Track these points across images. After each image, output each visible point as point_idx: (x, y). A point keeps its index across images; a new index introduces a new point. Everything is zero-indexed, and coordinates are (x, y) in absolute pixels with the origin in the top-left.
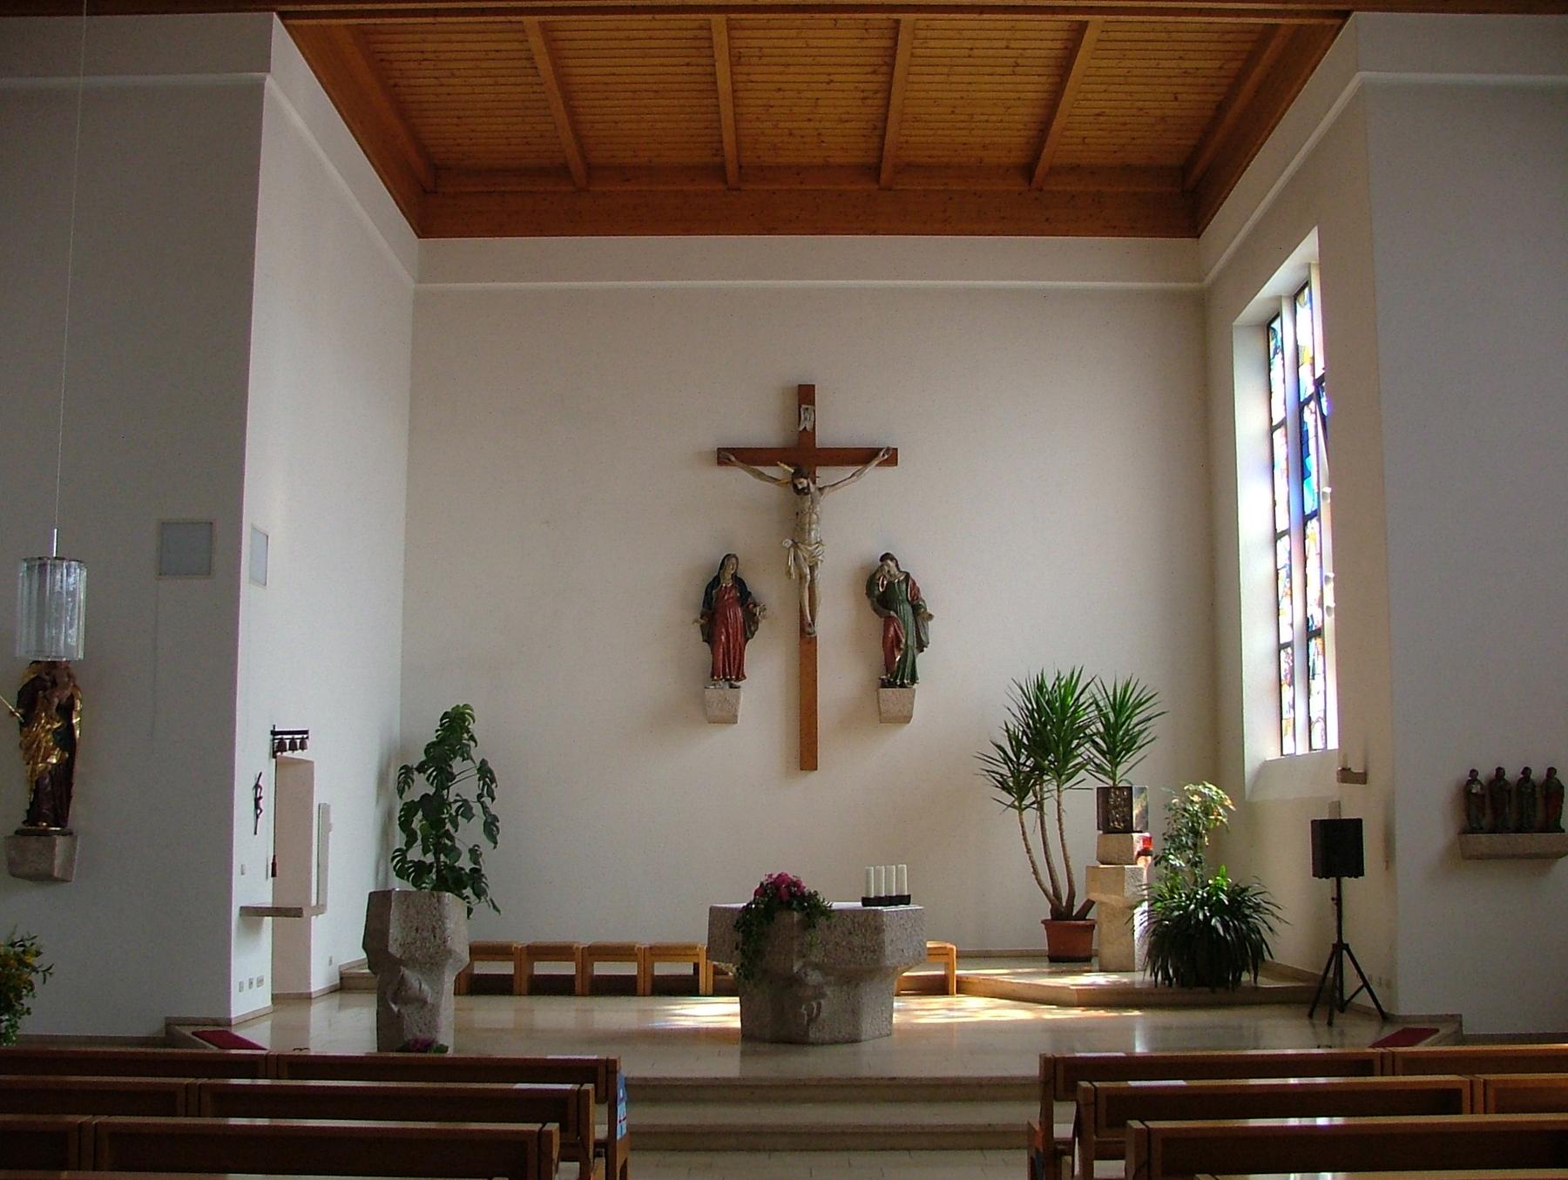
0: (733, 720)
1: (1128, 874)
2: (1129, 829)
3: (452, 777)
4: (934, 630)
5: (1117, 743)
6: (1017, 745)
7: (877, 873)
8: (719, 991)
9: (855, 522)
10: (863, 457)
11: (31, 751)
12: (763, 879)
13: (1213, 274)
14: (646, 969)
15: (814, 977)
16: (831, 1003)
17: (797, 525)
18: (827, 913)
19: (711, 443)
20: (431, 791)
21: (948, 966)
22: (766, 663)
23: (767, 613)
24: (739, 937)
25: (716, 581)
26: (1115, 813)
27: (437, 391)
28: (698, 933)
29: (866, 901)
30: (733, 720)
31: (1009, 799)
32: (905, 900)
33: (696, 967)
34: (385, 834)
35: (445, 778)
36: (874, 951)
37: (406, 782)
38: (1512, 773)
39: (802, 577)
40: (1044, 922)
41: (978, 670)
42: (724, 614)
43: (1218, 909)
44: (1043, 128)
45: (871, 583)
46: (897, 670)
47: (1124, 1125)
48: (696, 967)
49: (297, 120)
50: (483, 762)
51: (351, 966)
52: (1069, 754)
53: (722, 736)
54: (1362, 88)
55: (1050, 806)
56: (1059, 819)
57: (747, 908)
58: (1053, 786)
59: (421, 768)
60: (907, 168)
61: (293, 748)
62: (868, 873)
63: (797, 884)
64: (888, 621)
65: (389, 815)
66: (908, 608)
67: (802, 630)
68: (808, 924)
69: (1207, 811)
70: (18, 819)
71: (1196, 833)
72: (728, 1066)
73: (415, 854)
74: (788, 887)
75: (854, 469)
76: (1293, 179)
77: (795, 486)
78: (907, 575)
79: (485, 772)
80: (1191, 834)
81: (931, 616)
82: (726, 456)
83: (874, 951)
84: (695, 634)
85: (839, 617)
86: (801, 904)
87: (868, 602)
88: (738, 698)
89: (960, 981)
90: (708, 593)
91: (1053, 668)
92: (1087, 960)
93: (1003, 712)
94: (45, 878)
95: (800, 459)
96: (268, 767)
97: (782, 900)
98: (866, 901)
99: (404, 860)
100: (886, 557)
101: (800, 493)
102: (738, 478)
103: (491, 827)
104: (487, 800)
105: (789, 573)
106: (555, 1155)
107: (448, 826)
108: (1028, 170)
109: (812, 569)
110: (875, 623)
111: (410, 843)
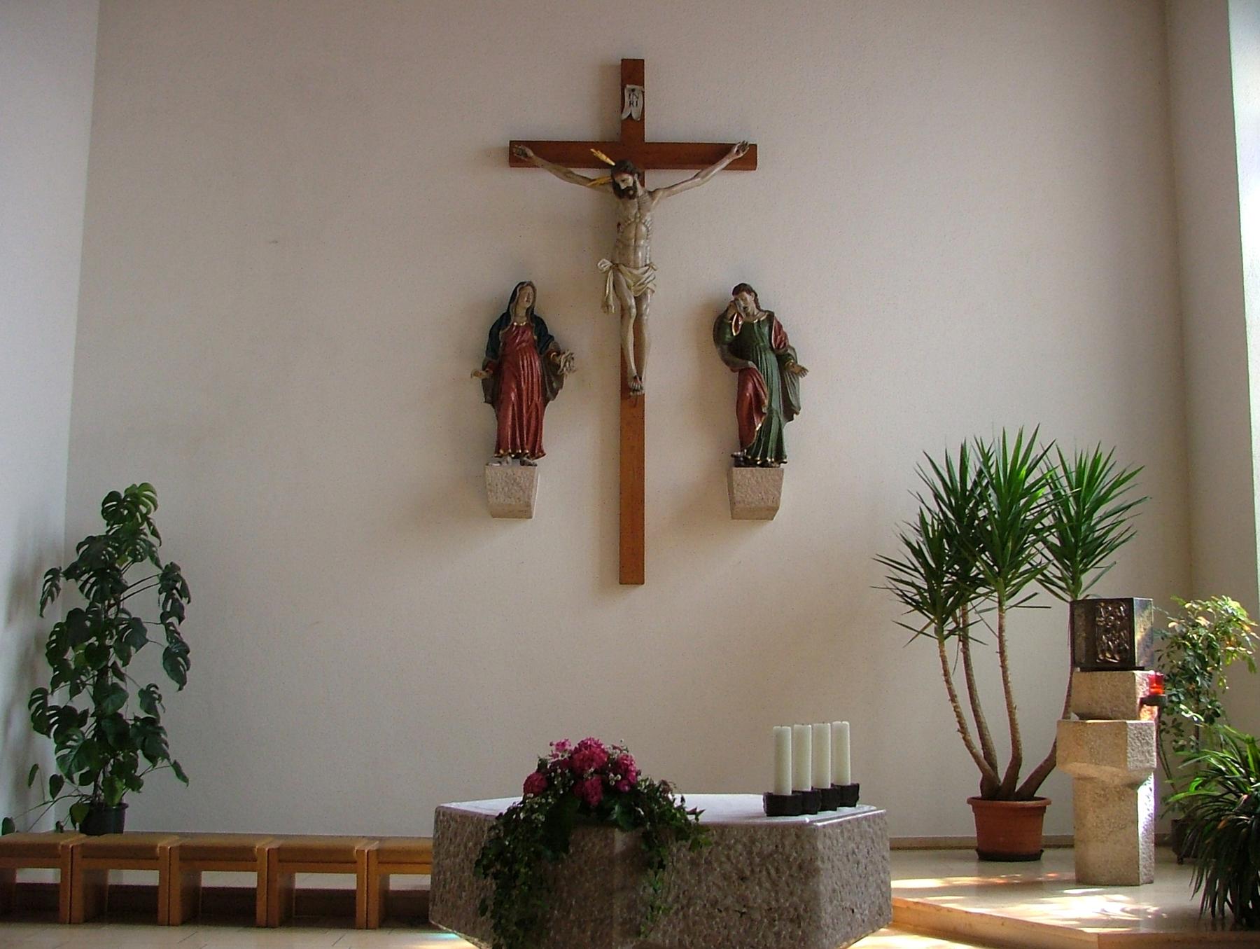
0: (524, 512)
1: (1132, 733)
2: (1128, 664)
4: (807, 390)
5: (1078, 549)
7: (799, 739)
9: (694, 244)
10: (702, 156)
12: (546, 753)
17: (618, 240)
18: (686, 829)
19: (502, 139)
20: (84, 604)
22: (574, 434)
23: (576, 364)
25: (505, 319)
26: (1100, 640)
30: (524, 512)
32: (845, 795)
34: (25, 667)
36: (797, 920)
37: (50, 593)
39: (624, 310)
40: (972, 801)
41: (881, 428)
42: (516, 365)
45: (720, 324)
46: (756, 440)
53: (507, 539)
56: (1002, 653)
57: (508, 819)
58: (992, 602)
59: (72, 573)
62: (779, 740)
63: (622, 766)
66: (772, 358)
73: (58, 698)
74: (602, 771)
75: (695, 172)
77: (616, 187)
78: (771, 316)
81: (803, 371)
82: (522, 153)
83: (797, 920)
84: (474, 391)
85: (675, 372)
86: (629, 811)
87: (714, 352)
88: (532, 480)
90: (493, 334)
95: (623, 156)
100: (741, 289)
102: (543, 184)
104: (174, 620)
105: (606, 305)
107: (113, 658)
109: (639, 300)
110: (724, 379)
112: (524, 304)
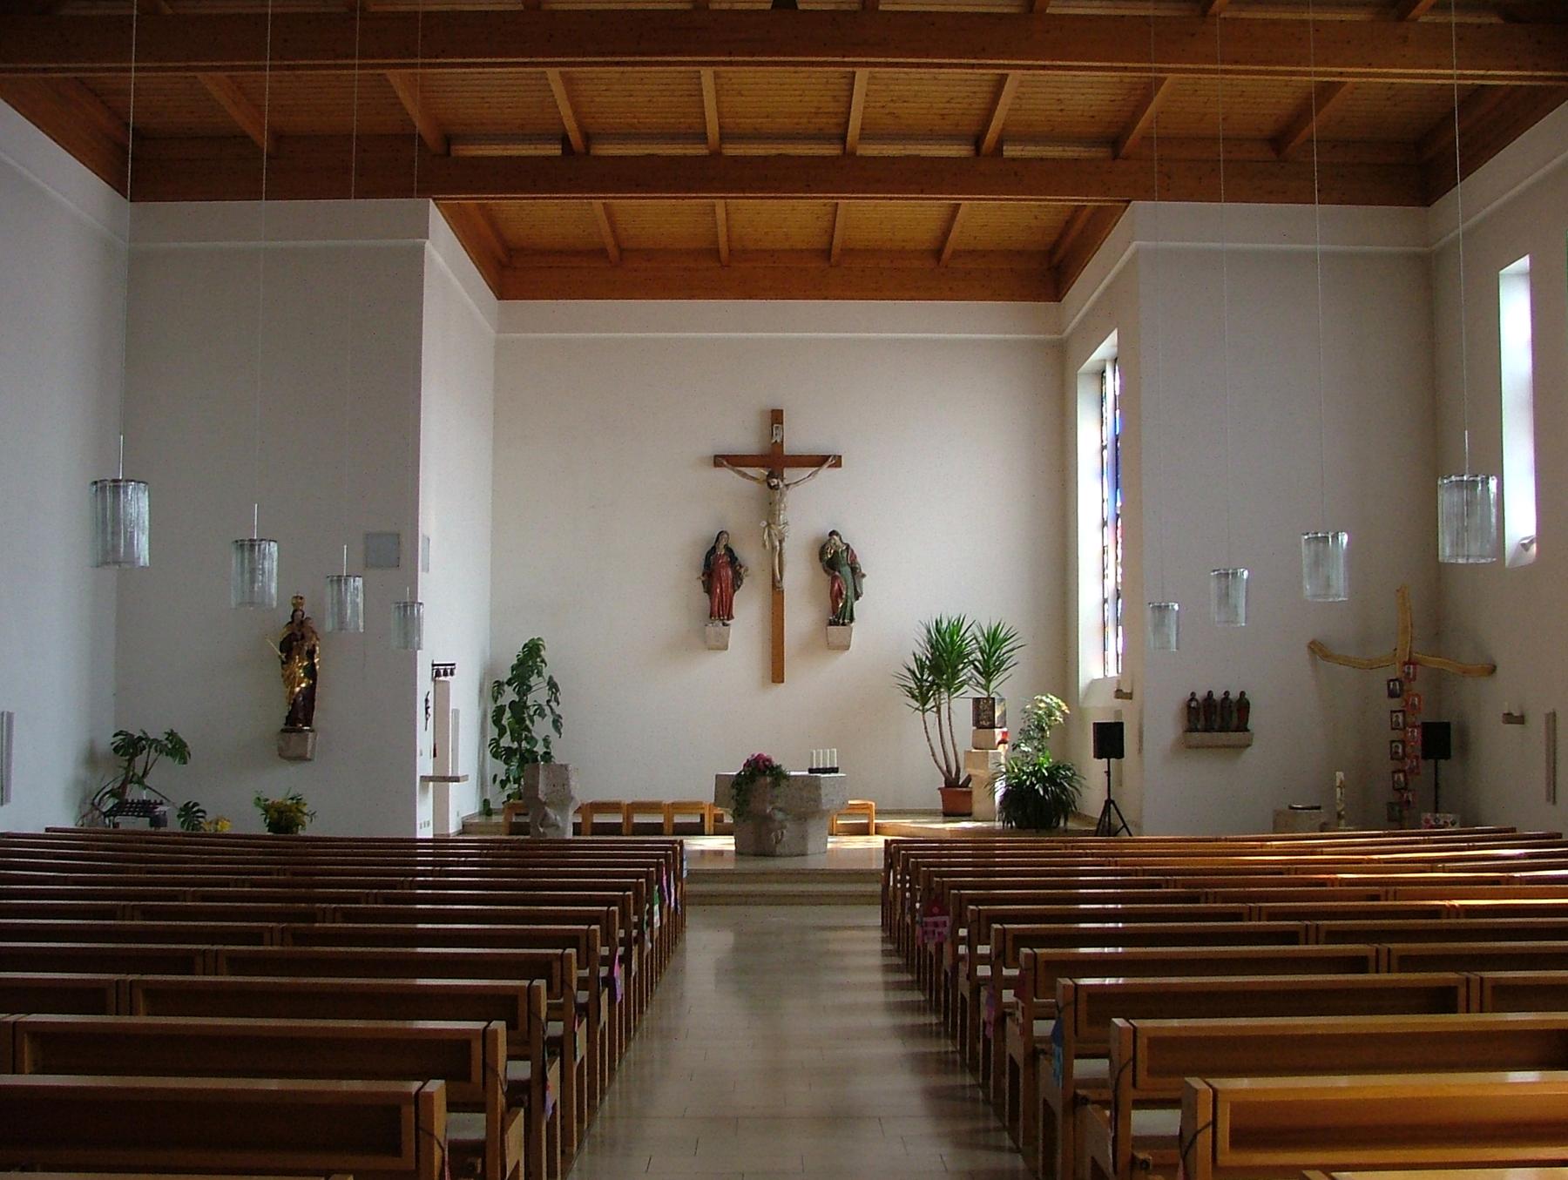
2: (993, 727)
3: (530, 688)
5: (988, 670)
6: (921, 667)
8: (720, 831)
9: (810, 508)
10: (818, 461)
11: (290, 680)
13: (1069, 330)
14: (669, 818)
15: (779, 816)
16: (789, 832)
17: (770, 510)
18: (787, 777)
19: (710, 450)
21: (869, 816)
22: (748, 607)
24: (734, 792)
25: (714, 548)
26: (984, 715)
27: (510, 415)
28: (707, 794)
29: (811, 771)
30: (726, 648)
31: (917, 705)
32: (835, 770)
33: (702, 817)
35: (524, 689)
38: (1218, 695)
39: (774, 548)
41: (893, 617)
42: (719, 573)
43: (1041, 779)
44: (946, 232)
45: (822, 551)
46: (840, 614)
47: (1109, 1023)
48: (702, 817)
49: (439, 259)
50: (551, 678)
51: (471, 816)
52: (955, 674)
54: (1137, 251)
55: (944, 708)
58: (945, 695)
59: (509, 683)
60: (848, 252)
61: (445, 674)
63: (769, 760)
64: (834, 578)
65: (484, 716)
67: (774, 586)
68: (776, 784)
69: (1050, 714)
70: (281, 723)
71: (1043, 730)
72: (730, 866)
73: (506, 741)
76: (1108, 288)
78: (848, 547)
79: (552, 685)
80: (1038, 728)
82: (720, 460)
85: (799, 575)
87: (819, 566)
89: (877, 826)
91: (949, 614)
92: (970, 814)
93: (915, 645)
94: (302, 758)
95: (772, 463)
96: (430, 686)
97: (760, 770)
98: (811, 771)
99: (498, 746)
100: (833, 533)
101: (772, 486)
102: (727, 474)
103: (557, 723)
104: (553, 704)
106: (543, 1015)
108: (938, 253)
109: (781, 542)
111: (501, 734)
112: (723, 543)
